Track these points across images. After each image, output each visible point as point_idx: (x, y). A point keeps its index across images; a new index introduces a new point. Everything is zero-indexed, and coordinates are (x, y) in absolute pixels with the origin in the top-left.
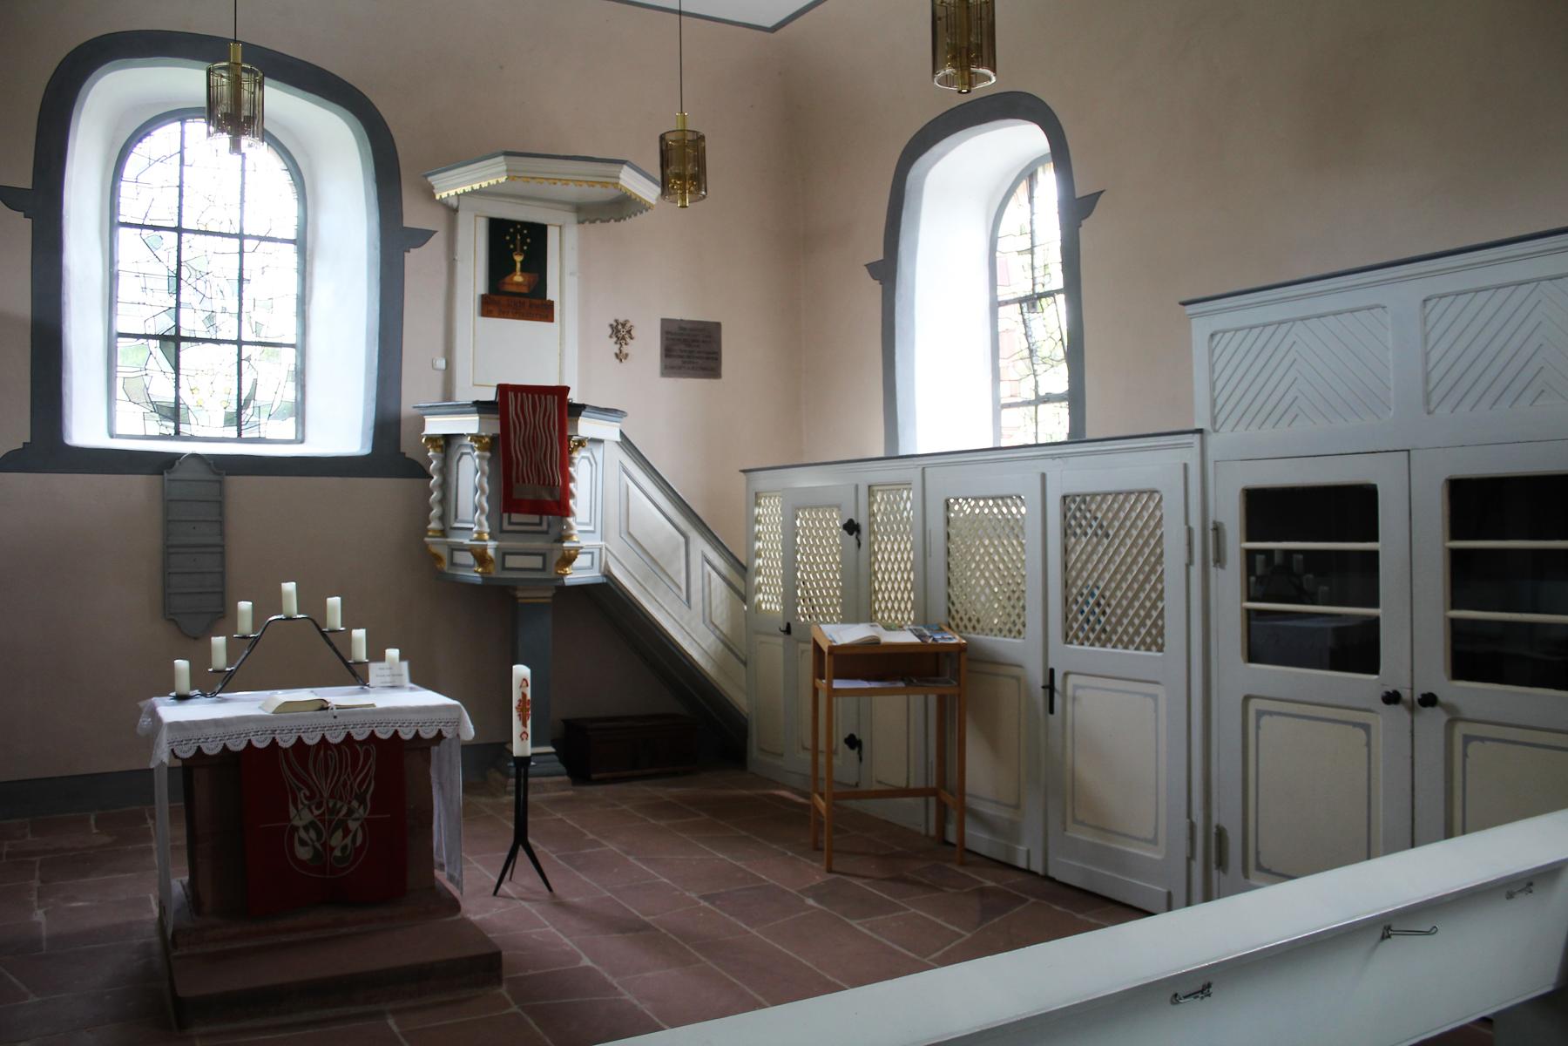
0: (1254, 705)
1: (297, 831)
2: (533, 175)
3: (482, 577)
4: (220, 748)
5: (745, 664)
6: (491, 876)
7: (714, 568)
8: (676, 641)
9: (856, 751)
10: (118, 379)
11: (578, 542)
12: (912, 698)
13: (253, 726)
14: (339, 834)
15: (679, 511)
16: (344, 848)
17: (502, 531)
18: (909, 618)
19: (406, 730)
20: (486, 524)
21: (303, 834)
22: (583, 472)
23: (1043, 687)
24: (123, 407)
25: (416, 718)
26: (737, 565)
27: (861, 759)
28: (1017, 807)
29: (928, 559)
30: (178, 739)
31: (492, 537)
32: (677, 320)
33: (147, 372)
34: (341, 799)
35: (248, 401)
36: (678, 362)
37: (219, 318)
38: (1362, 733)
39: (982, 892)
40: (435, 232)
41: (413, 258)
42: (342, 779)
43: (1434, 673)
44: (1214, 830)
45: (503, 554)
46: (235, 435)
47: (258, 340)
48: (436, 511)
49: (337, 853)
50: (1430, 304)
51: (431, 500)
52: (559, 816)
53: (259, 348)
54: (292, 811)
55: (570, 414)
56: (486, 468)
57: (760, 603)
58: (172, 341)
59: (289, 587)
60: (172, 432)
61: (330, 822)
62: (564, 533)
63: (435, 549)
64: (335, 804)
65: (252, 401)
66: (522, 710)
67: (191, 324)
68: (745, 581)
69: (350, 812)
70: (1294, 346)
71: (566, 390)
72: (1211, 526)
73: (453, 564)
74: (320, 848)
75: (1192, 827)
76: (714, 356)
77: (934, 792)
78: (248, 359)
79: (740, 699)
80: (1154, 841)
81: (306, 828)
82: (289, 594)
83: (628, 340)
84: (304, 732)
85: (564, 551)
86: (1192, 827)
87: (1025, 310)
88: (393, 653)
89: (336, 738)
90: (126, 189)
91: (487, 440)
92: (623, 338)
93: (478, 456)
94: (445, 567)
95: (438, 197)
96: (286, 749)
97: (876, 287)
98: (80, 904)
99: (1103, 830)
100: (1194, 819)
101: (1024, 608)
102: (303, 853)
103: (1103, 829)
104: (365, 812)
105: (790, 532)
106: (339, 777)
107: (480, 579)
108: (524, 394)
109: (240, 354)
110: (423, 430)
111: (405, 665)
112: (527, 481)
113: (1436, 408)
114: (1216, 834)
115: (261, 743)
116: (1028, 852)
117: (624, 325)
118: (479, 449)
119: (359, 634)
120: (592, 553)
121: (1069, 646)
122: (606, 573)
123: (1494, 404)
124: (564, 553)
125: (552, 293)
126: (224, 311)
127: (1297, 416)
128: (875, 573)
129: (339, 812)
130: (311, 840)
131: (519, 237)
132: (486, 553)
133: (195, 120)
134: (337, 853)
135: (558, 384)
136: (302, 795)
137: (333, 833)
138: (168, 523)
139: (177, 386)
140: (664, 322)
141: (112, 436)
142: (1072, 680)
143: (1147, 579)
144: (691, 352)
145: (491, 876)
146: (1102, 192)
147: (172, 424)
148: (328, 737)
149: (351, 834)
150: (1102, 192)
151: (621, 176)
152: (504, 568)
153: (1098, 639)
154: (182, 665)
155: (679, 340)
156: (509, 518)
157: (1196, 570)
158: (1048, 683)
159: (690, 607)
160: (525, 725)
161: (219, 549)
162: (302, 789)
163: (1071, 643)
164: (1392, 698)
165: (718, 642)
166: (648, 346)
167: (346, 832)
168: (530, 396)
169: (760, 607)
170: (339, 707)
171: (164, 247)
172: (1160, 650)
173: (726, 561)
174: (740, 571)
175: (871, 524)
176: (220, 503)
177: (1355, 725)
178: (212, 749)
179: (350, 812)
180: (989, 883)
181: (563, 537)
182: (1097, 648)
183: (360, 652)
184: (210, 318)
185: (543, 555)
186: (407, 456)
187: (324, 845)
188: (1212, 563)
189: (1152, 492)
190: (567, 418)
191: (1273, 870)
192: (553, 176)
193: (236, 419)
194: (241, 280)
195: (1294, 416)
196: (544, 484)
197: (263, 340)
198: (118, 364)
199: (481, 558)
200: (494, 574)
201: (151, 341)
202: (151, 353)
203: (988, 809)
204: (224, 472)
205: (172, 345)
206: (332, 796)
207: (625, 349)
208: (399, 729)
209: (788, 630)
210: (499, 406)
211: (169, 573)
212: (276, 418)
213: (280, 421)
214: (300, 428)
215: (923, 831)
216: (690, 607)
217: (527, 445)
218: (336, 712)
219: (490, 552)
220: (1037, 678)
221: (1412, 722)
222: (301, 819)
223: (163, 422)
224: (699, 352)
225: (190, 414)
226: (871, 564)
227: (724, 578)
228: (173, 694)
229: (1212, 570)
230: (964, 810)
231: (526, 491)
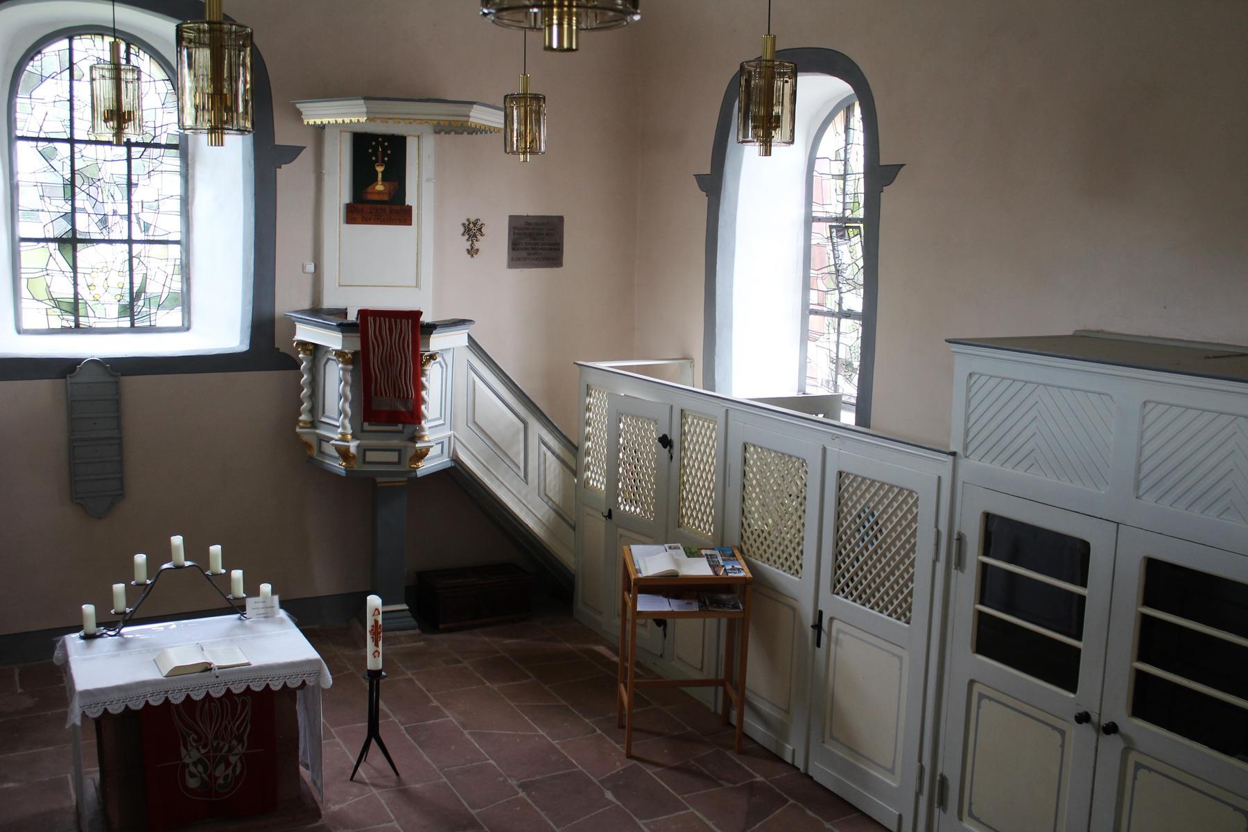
0: (977, 689)
1: (188, 767)
3: (345, 470)
4: (123, 708)
5: (574, 528)
6: (350, 757)
7: (549, 448)
8: (515, 514)
9: (662, 628)
10: (22, 280)
12: (707, 620)
13: (149, 689)
14: (222, 766)
16: (226, 777)
17: (363, 431)
18: (710, 530)
19: (276, 683)
20: (348, 426)
21: (192, 769)
22: (433, 377)
23: (812, 626)
24: (27, 304)
25: (284, 672)
26: (569, 445)
27: (665, 635)
28: (787, 711)
29: (727, 488)
30: (89, 704)
31: (354, 437)
33: (49, 272)
34: (223, 739)
35: (139, 293)
36: (523, 254)
38: (1058, 736)
39: (752, 789)
40: (304, 147)
41: (286, 175)
42: (223, 725)
43: (1117, 708)
44: (938, 778)
45: (363, 450)
46: (128, 324)
47: (146, 238)
48: (305, 406)
49: (221, 781)
50: (1149, 406)
52: (409, 675)
54: (183, 752)
55: (422, 333)
56: (349, 378)
57: (588, 479)
58: (70, 242)
59: (177, 540)
60: (73, 325)
61: (215, 758)
62: (416, 434)
63: (305, 438)
64: (218, 744)
65: (143, 294)
66: (374, 634)
67: (84, 225)
69: (230, 750)
70: (1037, 405)
71: (419, 313)
72: (955, 537)
73: (321, 452)
74: (206, 778)
75: (922, 769)
76: (557, 247)
77: (721, 683)
79: (568, 558)
80: (892, 771)
81: (195, 764)
82: (178, 547)
83: (479, 237)
84: (192, 691)
85: (417, 450)
86: (922, 769)
87: (834, 234)
88: (266, 588)
89: (217, 693)
91: (350, 355)
92: (475, 236)
93: (342, 369)
94: (315, 453)
95: (306, 123)
96: (177, 705)
97: (702, 199)
98: (11, 785)
100: (924, 763)
101: (802, 552)
102: (192, 783)
103: (853, 750)
104: (243, 747)
105: (615, 434)
106: (221, 724)
107: (344, 472)
108: (382, 318)
109: (130, 252)
110: (294, 334)
111: (276, 598)
113: (1143, 495)
114: (940, 781)
115: (156, 702)
116: (794, 751)
117: (475, 224)
118: (342, 362)
119: (237, 574)
121: (836, 596)
123: (1189, 507)
124: (417, 451)
125: (410, 200)
127: (1033, 464)
128: (684, 484)
129: (221, 750)
130: (199, 772)
131: (380, 150)
132: (349, 452)
133: (82, 37)
134: (221, 781)
136: (191, 739)
137: (216, 766)
139: (75, 284)
141: (20, 331)
142: (836, 624)
143: (902, 561)
144: (536, 244)
145: (350, 757)
148: (211, 693)
149: (231, 767)
150: (903, 165)
151: (471, 114)
152: (365, 462)
153: (860, 598)
154: (89, 609)
155: (525, 234)
157: (941, 566)
158: (817, 622)
159: (527, 484)
160: (377, 645)
162: (191, 734)
163: (838, 594)
164: (1083, 718)
165: (551, 511)
166: (497, 240)
167: (228, 764)
168: (387, 320)
169: (589, 484)
170: (220, 668)
171: (58, 158)
172: (908, 623)
174: (572, 451)
175: (682, 442)
177: (1054, 728)
178: (116, 709)
179: (230, 750)
180: (759, 778)
181: (415, 437)
182: (857, 605)
183: (239, 590)
184: (104, 221)
185: (399, 451)
186: (281, 351)
187: (210, 776)
188: (953, 567)
189: (911, 492)
190: (420, 336)
191: (981, 820)
192: (410, 117)
194: (130, 185)
195: (1030, 464)
196: (399, 396)
197: (151, 238)
199: (344, 454)
200: (356, 468)
201: (50, 244)
202: (51, 255)
203: (765, 708)
205: (69, 247)
206: (216, 738)
207: (477, 245)
208: (270, 683)
209: (609, 515)
210: (360, 328)
211: (74, 464)
212: (165, 308)
214: (186, 316)
215: (712, 710)
218: (218, 672)
219: (353, 450)
220: (809, 618)
221: (1098, 740)
222: (190, 757)
223: (64, 317)
224: (543, 244)
225: (88, 308)
226: (681, 476)
227: (558, 457)
228: (82, 633)
229: (954, 572)
230: (744, 701)
231: (384, 403)
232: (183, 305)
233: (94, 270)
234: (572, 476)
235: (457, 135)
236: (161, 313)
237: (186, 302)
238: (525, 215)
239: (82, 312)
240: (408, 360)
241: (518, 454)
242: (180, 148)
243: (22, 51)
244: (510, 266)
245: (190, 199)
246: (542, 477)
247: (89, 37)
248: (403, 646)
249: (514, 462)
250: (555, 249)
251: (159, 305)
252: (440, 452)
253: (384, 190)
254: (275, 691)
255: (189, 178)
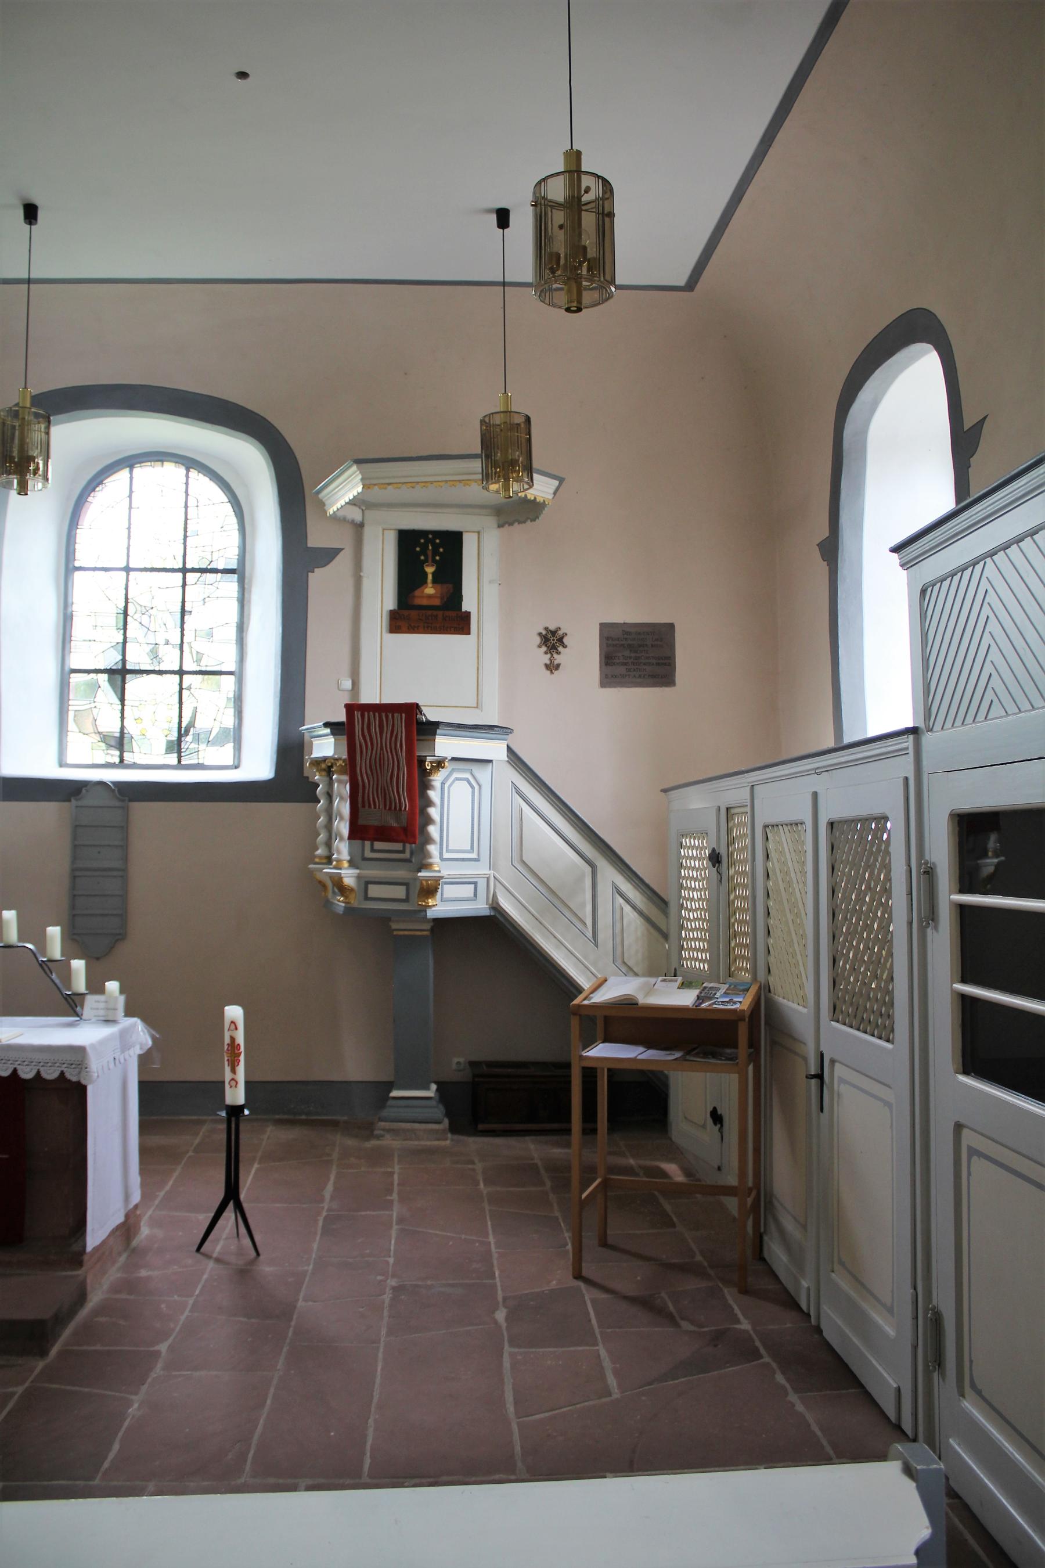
0: (968, 1138)
2: (387, 481)
7: (627, 901)
9: (719, 1126)
11: (439, 871)
15: (582, 836)
17: (364, 859)
31: (352, 864)
32: (621, 624)
36: (622, 670)
37: (163, 650)
41: (317, 579)
45: (366, 883)
46: (175, 762)
47: (198, 669)
48: (322, 837)
51: (318, 825)
53: (200, 677)
58: (119, 675)
60: (117, 760)
65: (192, 729)
67: (136, 658)
68: (667, 917)
76: (666, 661)
78: (189, 688)
83: (560, 649)
90: (82, 535)
97: (823, 567)
99: (858, 1281)
103: (857, 1280)
112: (373, 806)
120: (475, 883)
122: (495, 905)
125: (468, 604)
126: (167, 643)
131: (430, 548)
133: (142, 464)
135: (378, 702)
138: (76, 848)
139: (122, 718)
140: (603, 626)
144: (639, 658)
146: (985, 418)
147: (117, 753)
150: (985, 418)
152: (367, 898)
155: (622, 645)
156: (372, 846)
159: (597, 946)
161: (120, 873)
168: (377, 714)
173: (643, 893)
176: (124, 828)
183: (80, 984)
184: (155, 655)
185: (406, 885)
193: (176, 746)
194: (183, 612)
196: (390, 809)
197: (204, 669)
198: (71, 698)
201: (100, 675)
204: (127, 798)
205: (119, 678)
207: (558, 659)
213: (218, 748)
216: (597, 946)
217: (374, 767)
223: (109, 751)
227: (641, 913)
232: (234, 742)
233: (141, 702)
234: (662, 940)
235: (521, 525)
236: (212, 750)
237: (237, 738)
238: (622, 622)
239: (126, 747)
240: (401, 765)
241: (583, 905)
242: (237, 572)
243: (84, 483)
244: (603, 684)
245: (245, 626)
246: (618, 939)
247: (149, 464)
248: (423, 1143)
249: (576, 915)
250: (665, 664)
251: (209, 742)
252: (472, 895)
253: (435, 593)
254: (25, 1080)
255: (245, 602)
